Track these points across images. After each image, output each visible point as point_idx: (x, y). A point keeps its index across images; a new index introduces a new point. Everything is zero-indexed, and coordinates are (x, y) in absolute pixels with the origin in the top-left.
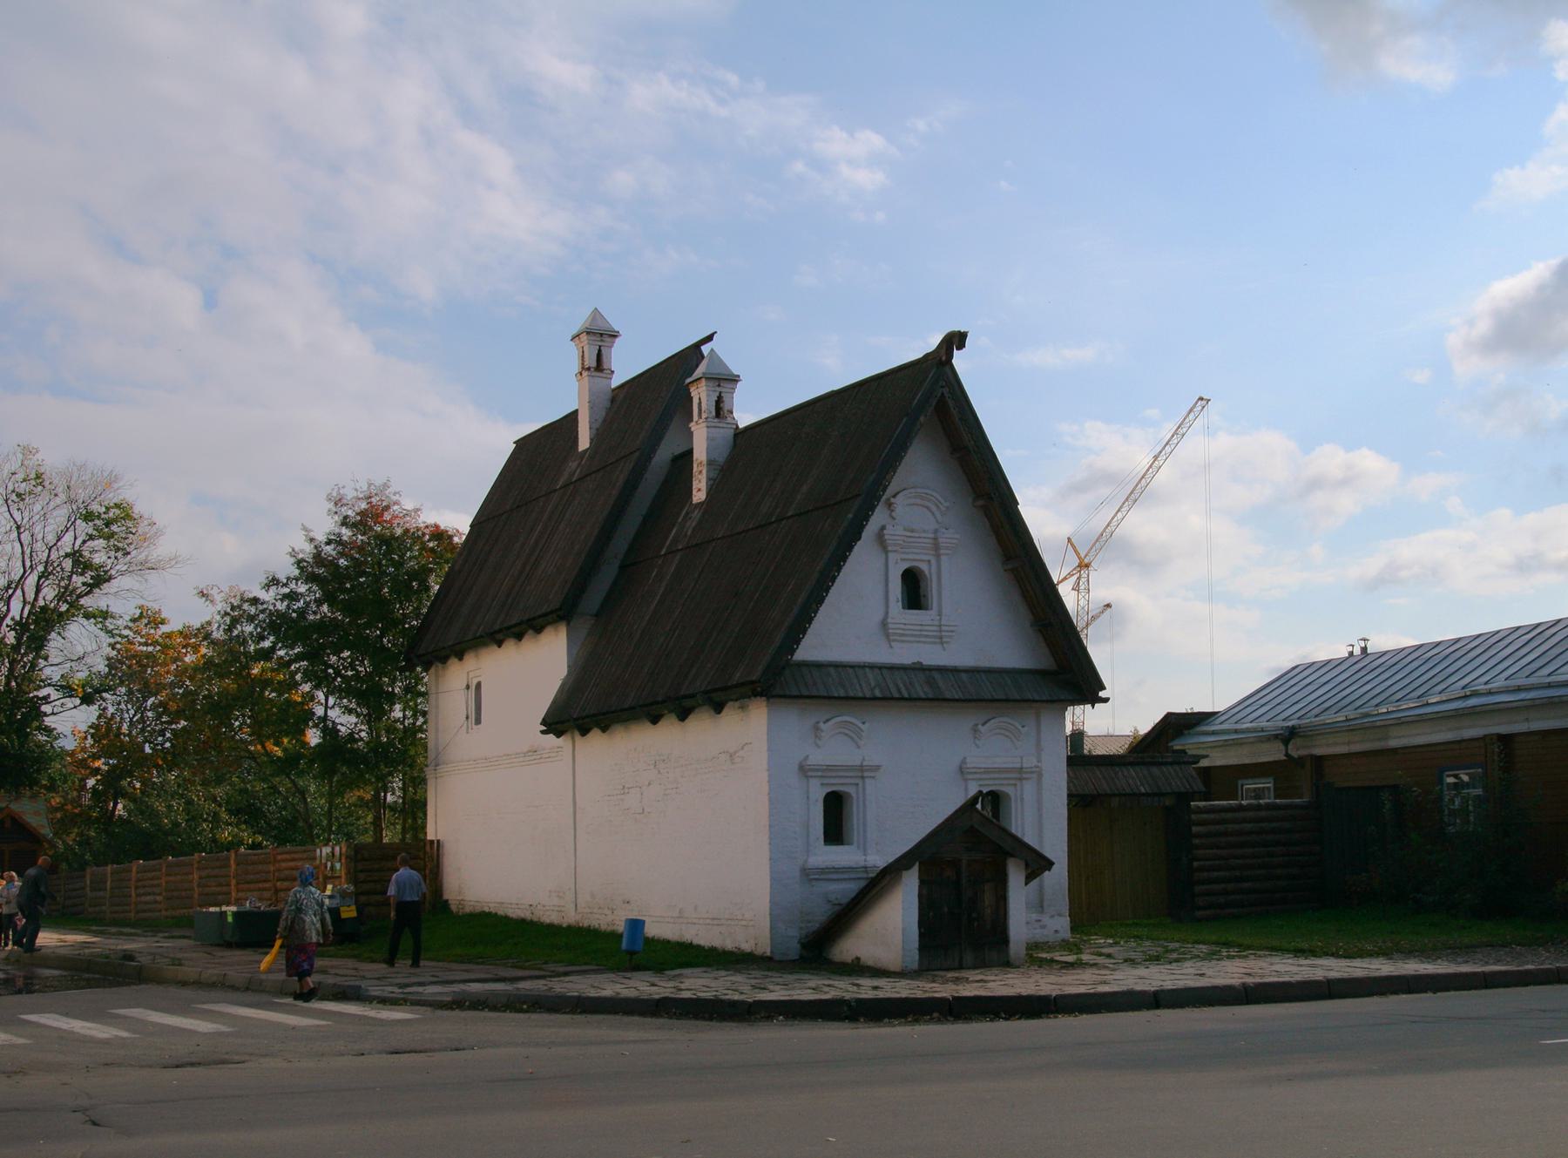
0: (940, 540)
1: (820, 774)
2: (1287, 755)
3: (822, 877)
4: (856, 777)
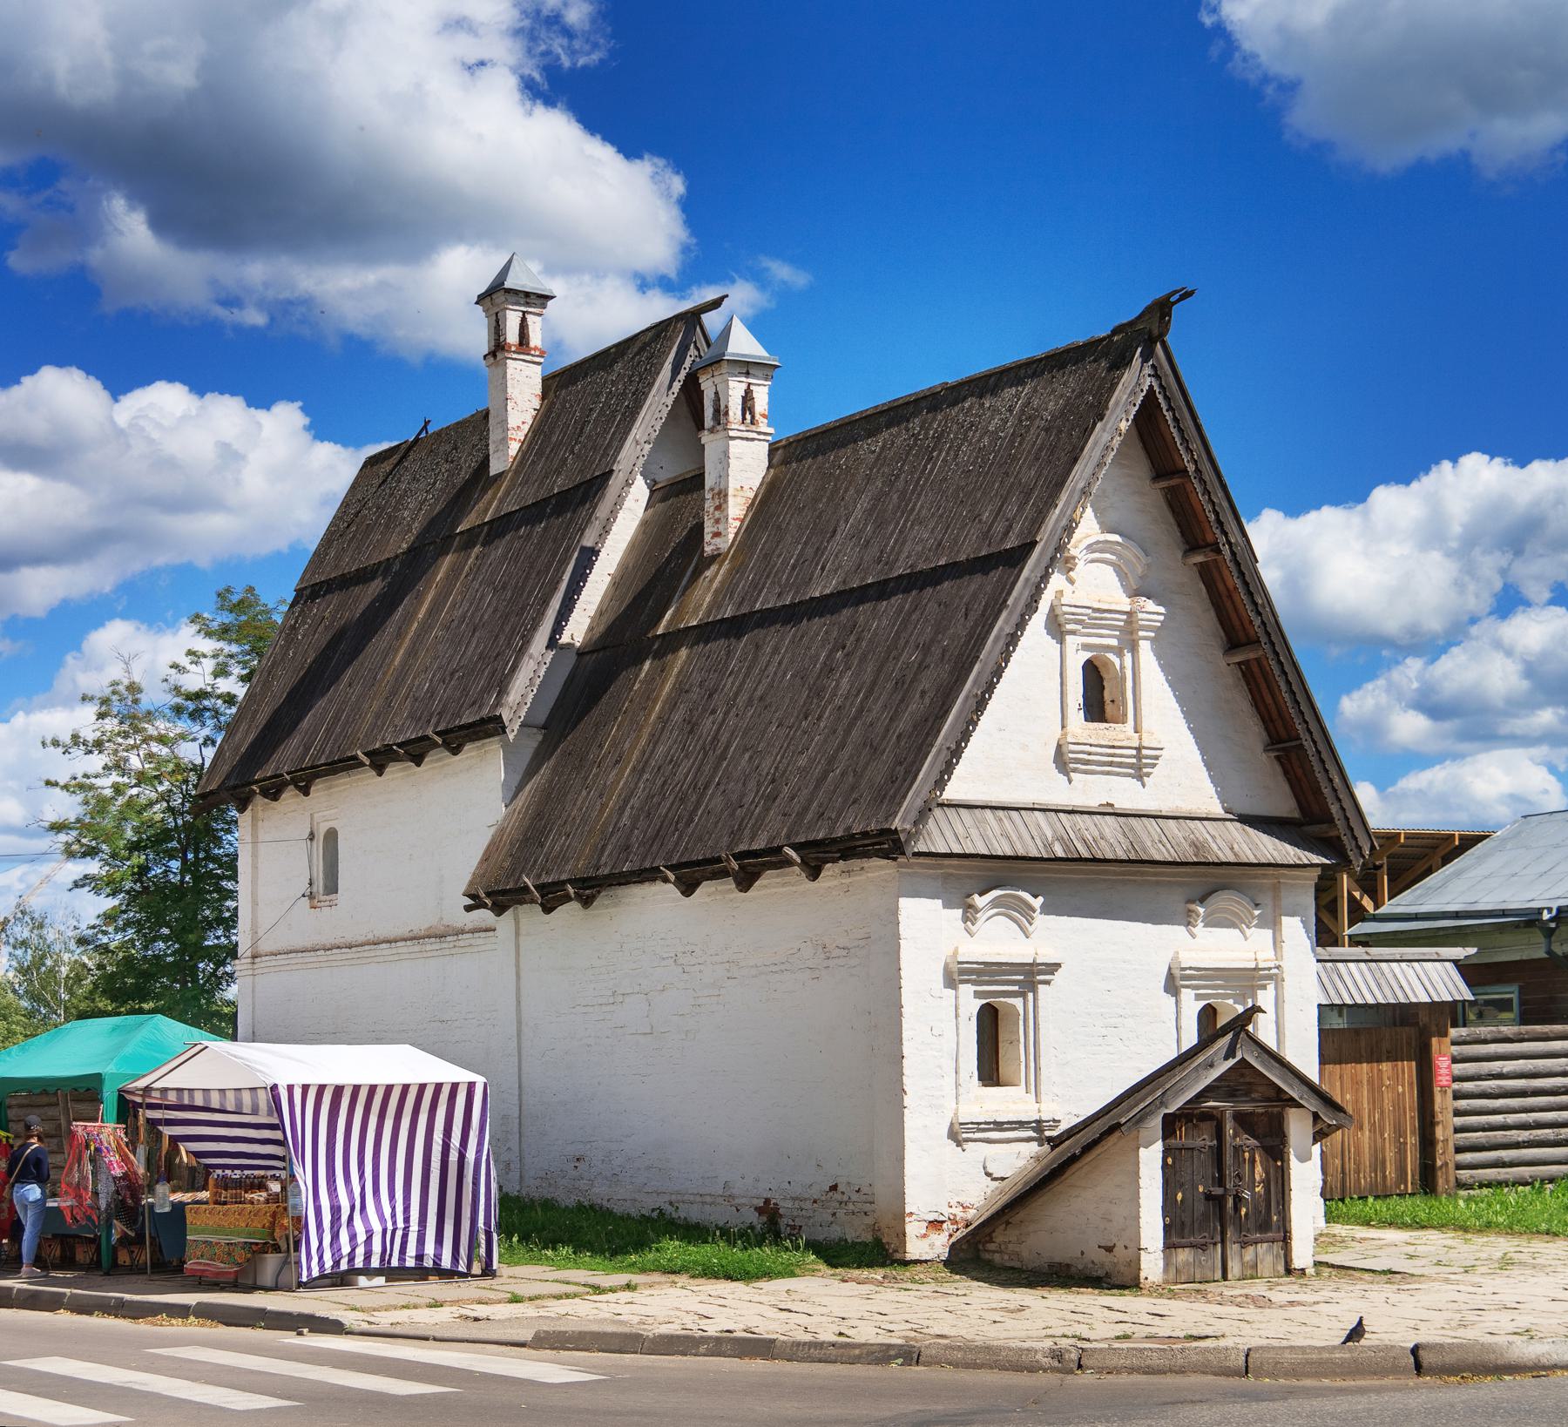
2: (1549, 952)
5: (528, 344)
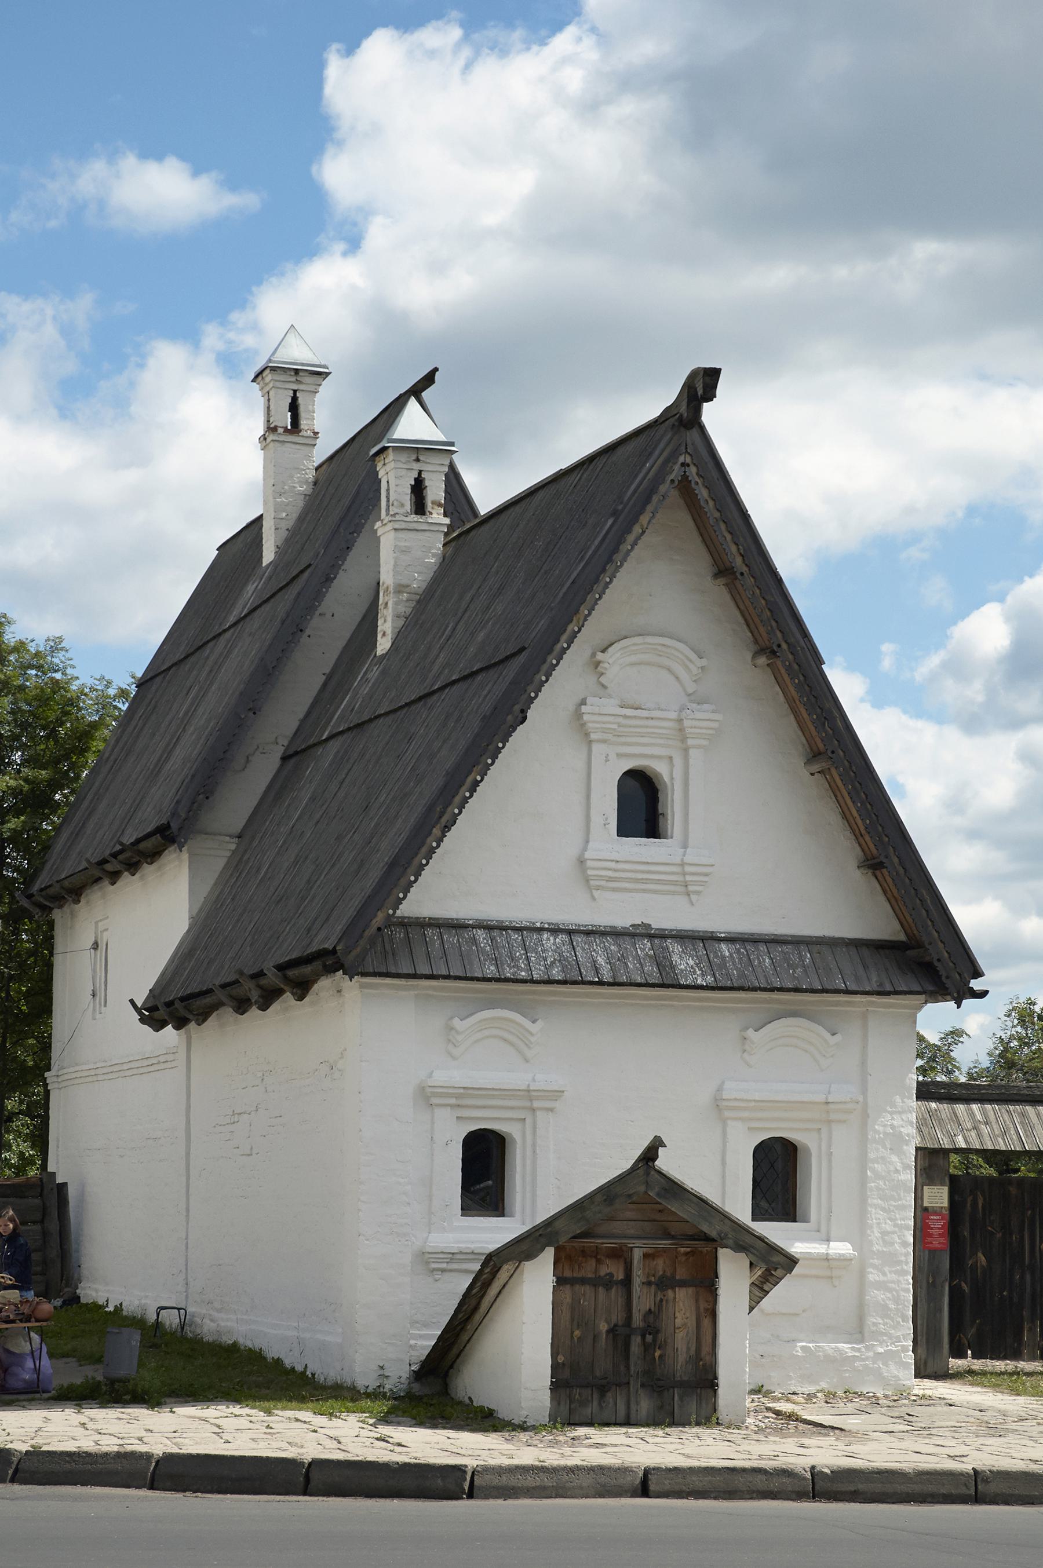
1: (453, 1101)
3: (455, 1266)
4: (524, 1108)
5: (304, 423)
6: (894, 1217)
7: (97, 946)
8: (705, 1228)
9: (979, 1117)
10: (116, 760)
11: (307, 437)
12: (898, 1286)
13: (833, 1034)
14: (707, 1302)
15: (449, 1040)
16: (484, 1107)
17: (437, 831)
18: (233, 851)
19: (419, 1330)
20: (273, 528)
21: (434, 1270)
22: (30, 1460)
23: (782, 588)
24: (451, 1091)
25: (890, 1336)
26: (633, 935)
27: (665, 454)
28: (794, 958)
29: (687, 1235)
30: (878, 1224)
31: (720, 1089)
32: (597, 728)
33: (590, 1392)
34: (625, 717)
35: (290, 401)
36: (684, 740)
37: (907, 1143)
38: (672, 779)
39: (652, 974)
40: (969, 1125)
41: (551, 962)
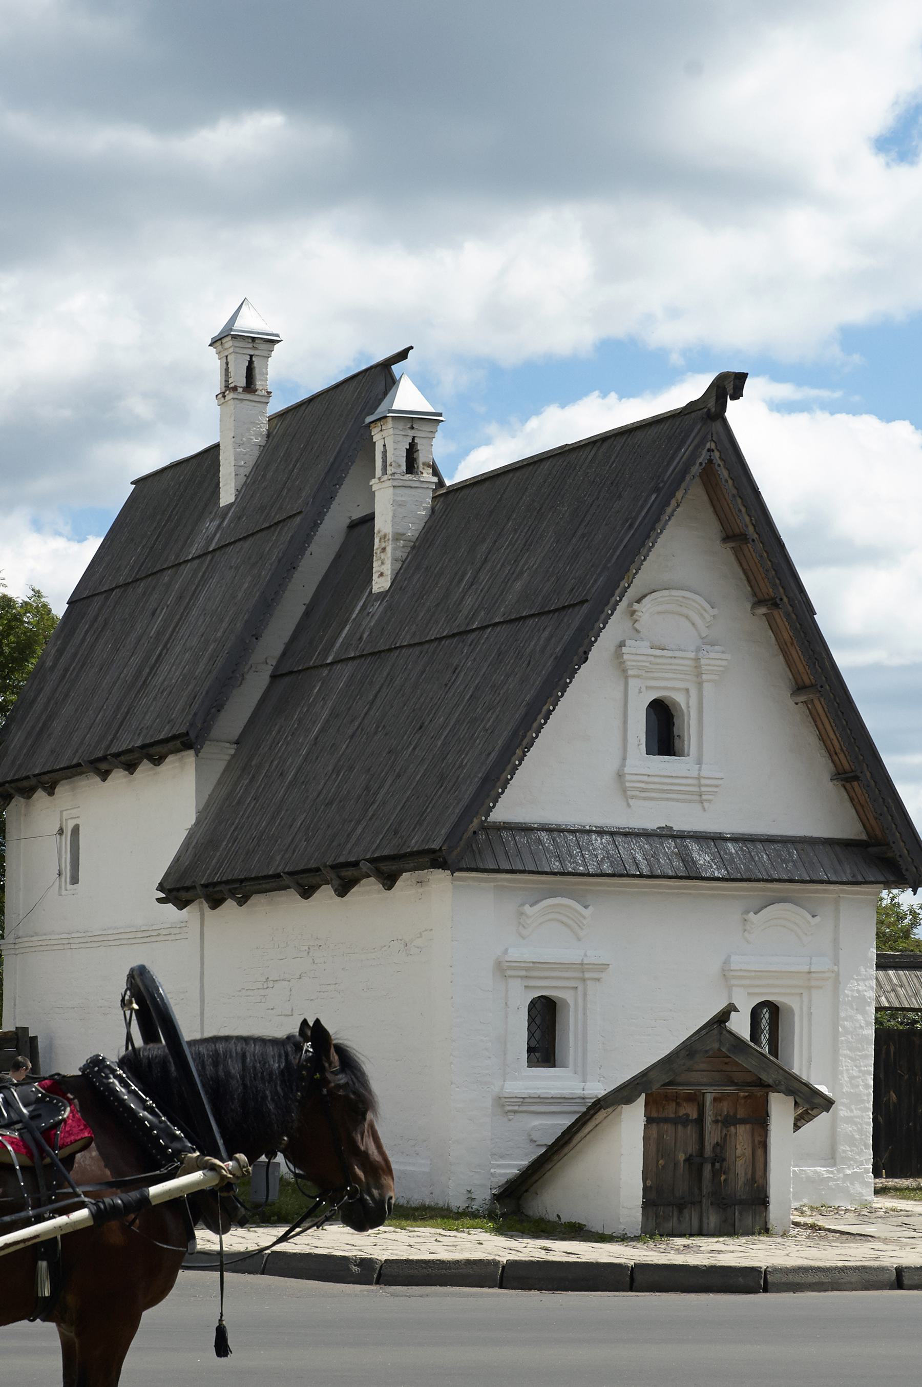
0: (703, 661)
1: (523, 973)
3: (524, 1108)
5: (259, 384)
6: (858, 1065)
7: (63, 832)
8: (764, 1076)
9: (895, 981)
10: (66, 670)
11: (262, 396)
12: (862, 1120)
13: (813, 916)
14: (760, 1136)
15: (520, 923)
16: (546, 978)
17: (519, 752)
18: (232, 755)
19: (496, 1161)
20: (233, 474)
21: (509, 1111)
22: (390, 1266)
23: (784, 552)
24: (523, 965)
25: (855, 1161)
26: (660, 836)
27: (696, 442)
28: (784, 854)
29: (747, 1083)
30: (847, 1070)
31: (727, 962)
32: (633, 666)
33: (671, 1209)
34: (655, 656)
35: (247, 365)
36: (699, 675)
37: (869, 1004)
38: (688, 707)
39: (680, 869)
40: (888, 988)
41: (602, 859)
